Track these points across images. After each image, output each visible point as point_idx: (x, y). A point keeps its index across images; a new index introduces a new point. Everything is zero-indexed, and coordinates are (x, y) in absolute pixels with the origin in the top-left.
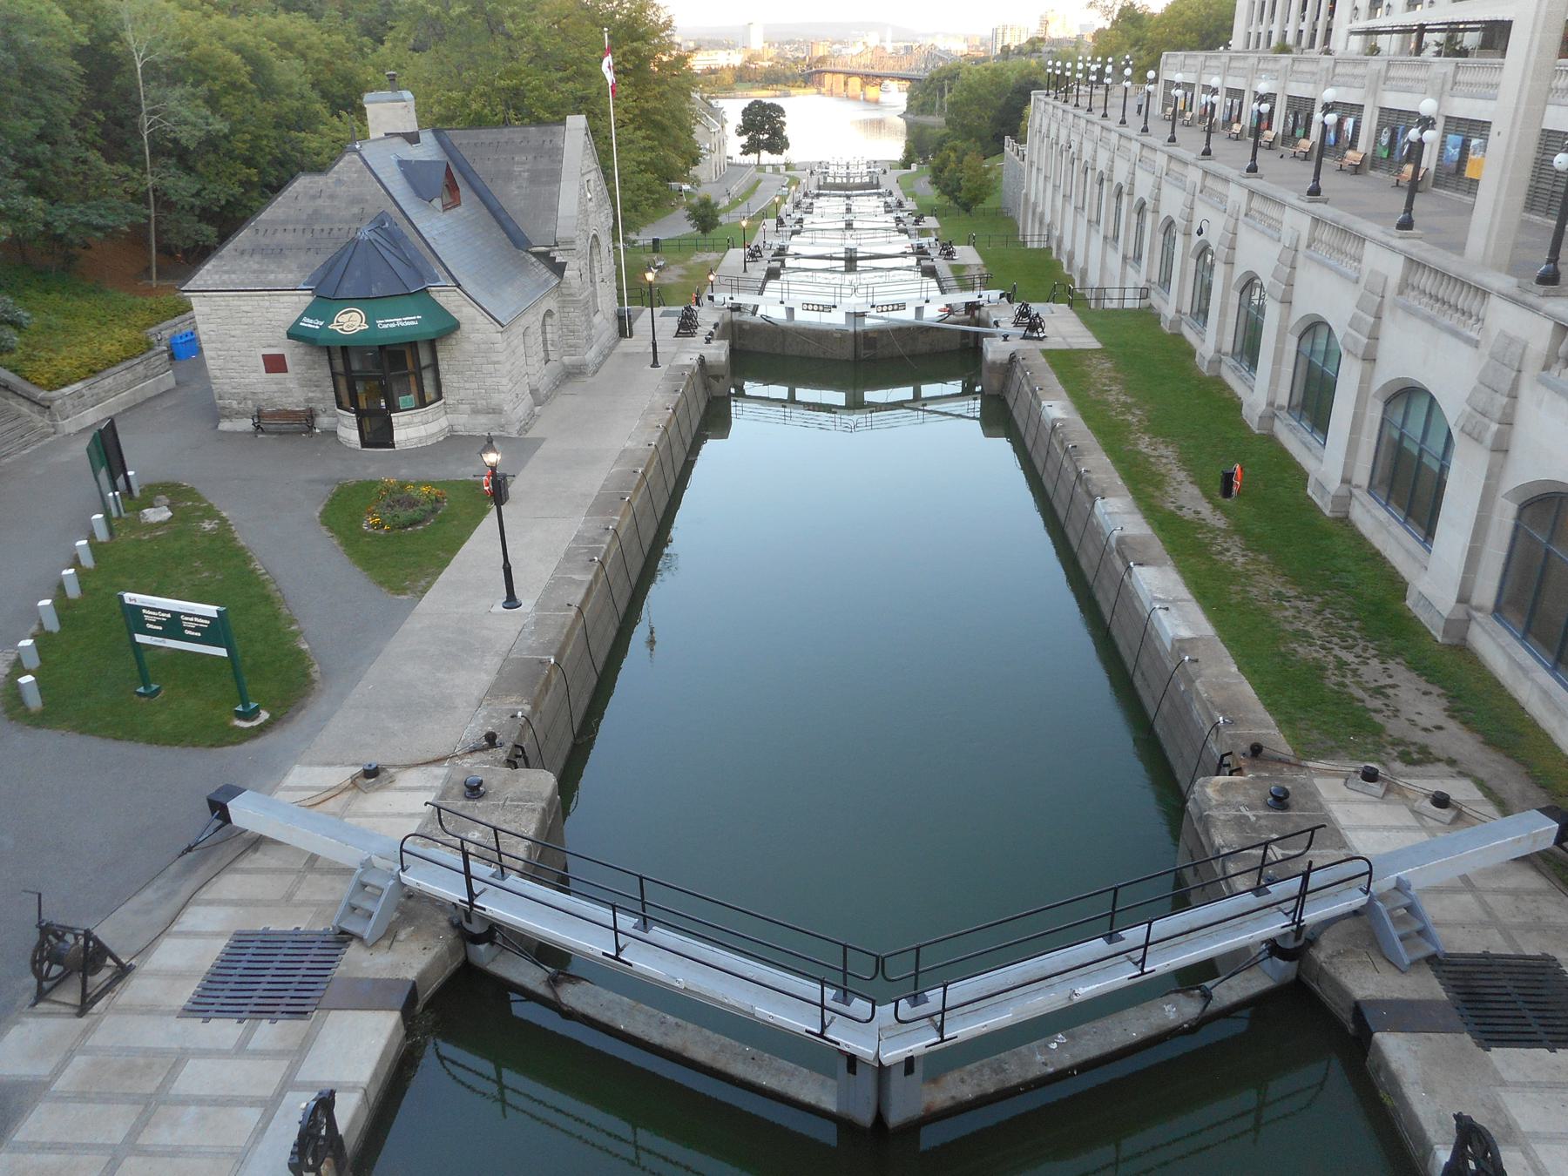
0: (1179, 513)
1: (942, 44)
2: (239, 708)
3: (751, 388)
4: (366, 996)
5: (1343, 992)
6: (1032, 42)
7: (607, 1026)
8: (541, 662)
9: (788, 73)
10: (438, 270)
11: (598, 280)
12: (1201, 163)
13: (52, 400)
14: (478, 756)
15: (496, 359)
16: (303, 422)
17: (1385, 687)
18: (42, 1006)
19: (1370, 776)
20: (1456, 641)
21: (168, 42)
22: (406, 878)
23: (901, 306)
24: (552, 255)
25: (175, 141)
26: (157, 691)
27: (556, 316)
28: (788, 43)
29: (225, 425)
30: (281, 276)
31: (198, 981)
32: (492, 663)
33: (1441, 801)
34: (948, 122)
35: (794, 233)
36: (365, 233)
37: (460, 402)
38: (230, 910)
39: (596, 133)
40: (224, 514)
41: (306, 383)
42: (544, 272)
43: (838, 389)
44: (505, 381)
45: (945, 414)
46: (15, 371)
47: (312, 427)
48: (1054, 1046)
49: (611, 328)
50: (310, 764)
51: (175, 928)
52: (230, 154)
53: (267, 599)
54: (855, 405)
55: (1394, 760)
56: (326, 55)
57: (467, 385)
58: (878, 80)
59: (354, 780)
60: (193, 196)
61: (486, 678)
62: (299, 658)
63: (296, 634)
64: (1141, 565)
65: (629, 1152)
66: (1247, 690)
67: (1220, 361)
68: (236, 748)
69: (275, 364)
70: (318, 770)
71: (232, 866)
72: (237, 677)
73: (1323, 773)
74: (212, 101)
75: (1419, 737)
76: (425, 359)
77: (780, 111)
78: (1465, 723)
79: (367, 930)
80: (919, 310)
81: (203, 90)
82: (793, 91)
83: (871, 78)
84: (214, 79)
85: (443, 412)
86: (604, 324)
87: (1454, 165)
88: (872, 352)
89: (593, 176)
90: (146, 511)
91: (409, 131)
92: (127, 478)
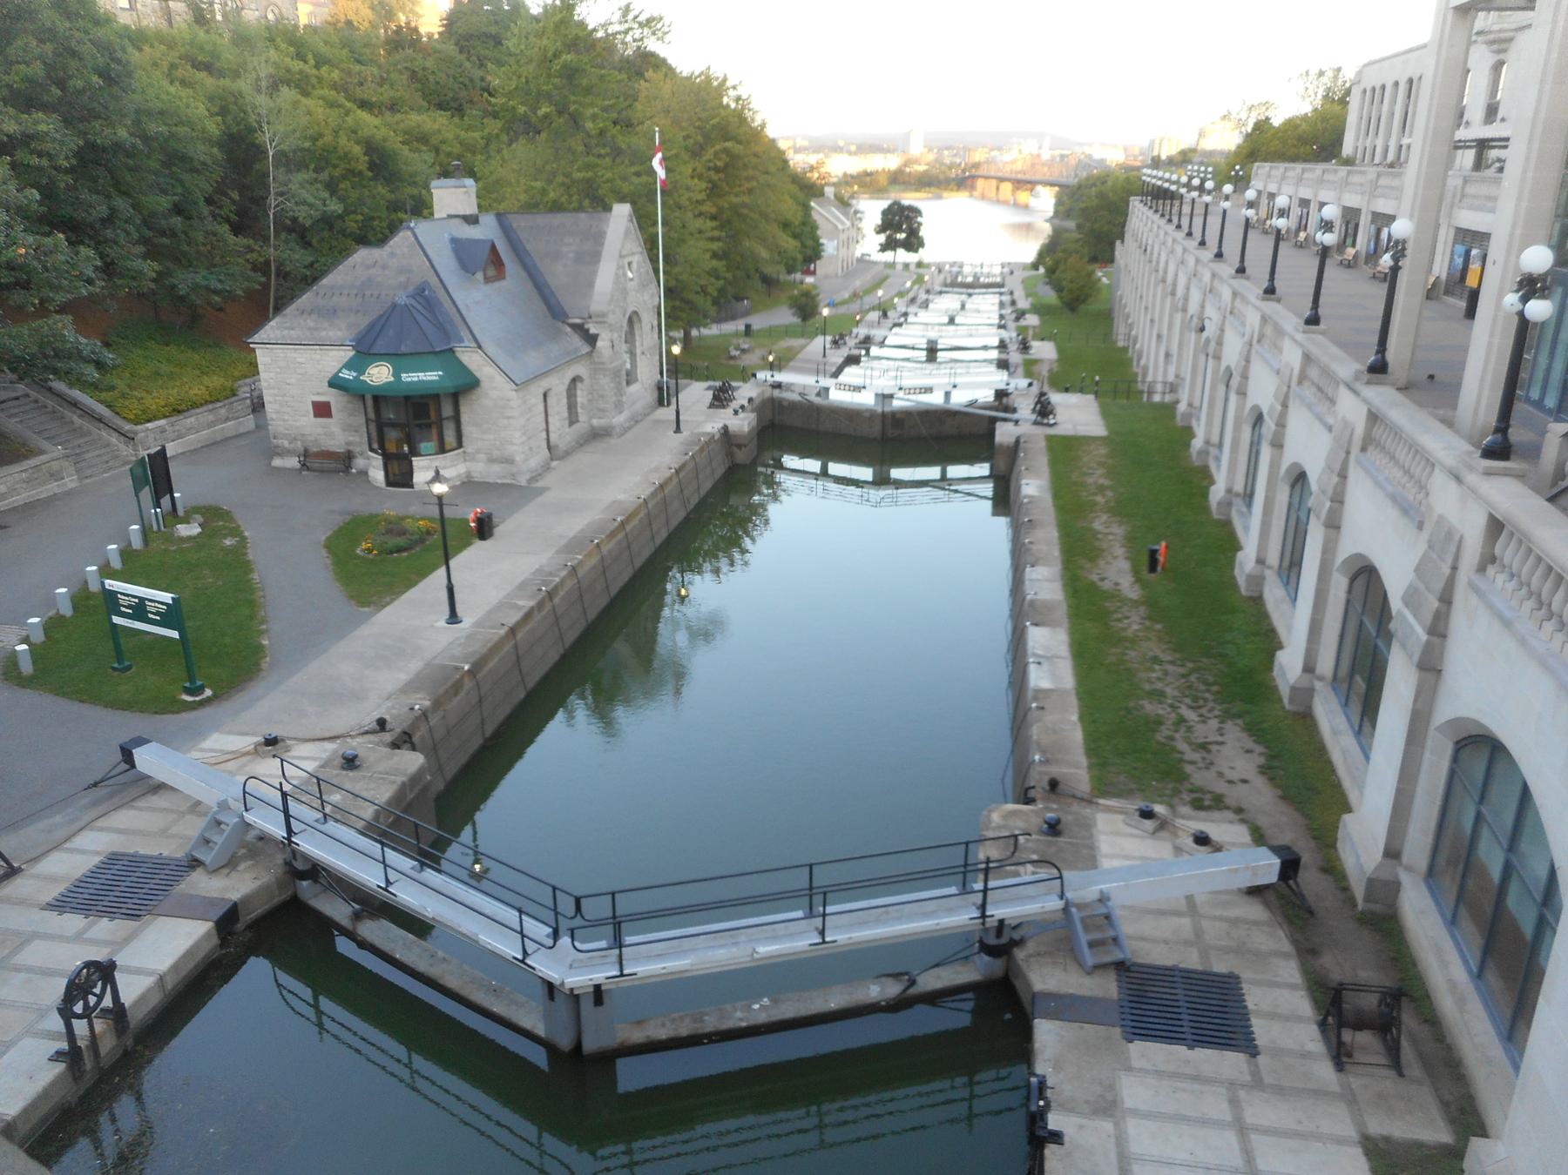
0: (1099, 583)
1: (1098, 154)
2: (187, 685)
3: (790, 461)
4: (189, 909)
5: (1028, 985)
6: (1184, 153)
7: (387, 954)
8: (457, 669)
9: (941, 177)
10: (464, 333)
11: (638, 351)
12: (1211, 264)
13: (136, 433)
16: (345, 460)
17: (1210, 743)
19: (1147, 814)
20: (1301, 709)
21: (298, 134)
22: (249, 817)
23: (929, 390)
25: (294, 220)
26: (129, 668)
27: (587, 381)
28: (947, 149)
30: (331, 334)
31: (67, 885)
32: (415, 666)
33: (1202, 840)
34: (1079, 227)
35: (895, 325)
36: (402, 299)
37: (478, 451)
38: (114, 836)
39: (643, 219)
40: (246, 534)
42: (576, 341)
44: (517, 434)
45: (969, 494)
46: (109, 407)
47: (349, 467)
48: (756, 1006)
49: (651, 396)
50: (229, 733)
51: (67, 845)
52: (343, 232)
53: (252, 603)
54: (882, 481)
55: (1185, 804)
56: (457, 149)
57: (485, 437)
58: (1029, 186)
59: (257, 745)
60: (306, 267)
61: (403, 677)
62: (258, 650)
63: (262, 632)
64: (1036, 625)
65: (405, 1073)
66: (1077, 736)
67: (1208, 453)
69: (322, 410)
70: (232, 738)
72: (187, 656)
73: (1109, 810)
74: (332, 187)
75: (1220, 787)
76: (447, 410)
77: (917, 212)
78: (1271, 779)
79: (206, 857)
80: (947, 394)
81: (324, 176)
82: (945, 194)
83: (1024, 183)
84: (335, 166)
86: (641, 392)
87: (1458, 274)
89: (636, 259)
90: (179, 526)
91: (468, 213)
92: (173, 498)
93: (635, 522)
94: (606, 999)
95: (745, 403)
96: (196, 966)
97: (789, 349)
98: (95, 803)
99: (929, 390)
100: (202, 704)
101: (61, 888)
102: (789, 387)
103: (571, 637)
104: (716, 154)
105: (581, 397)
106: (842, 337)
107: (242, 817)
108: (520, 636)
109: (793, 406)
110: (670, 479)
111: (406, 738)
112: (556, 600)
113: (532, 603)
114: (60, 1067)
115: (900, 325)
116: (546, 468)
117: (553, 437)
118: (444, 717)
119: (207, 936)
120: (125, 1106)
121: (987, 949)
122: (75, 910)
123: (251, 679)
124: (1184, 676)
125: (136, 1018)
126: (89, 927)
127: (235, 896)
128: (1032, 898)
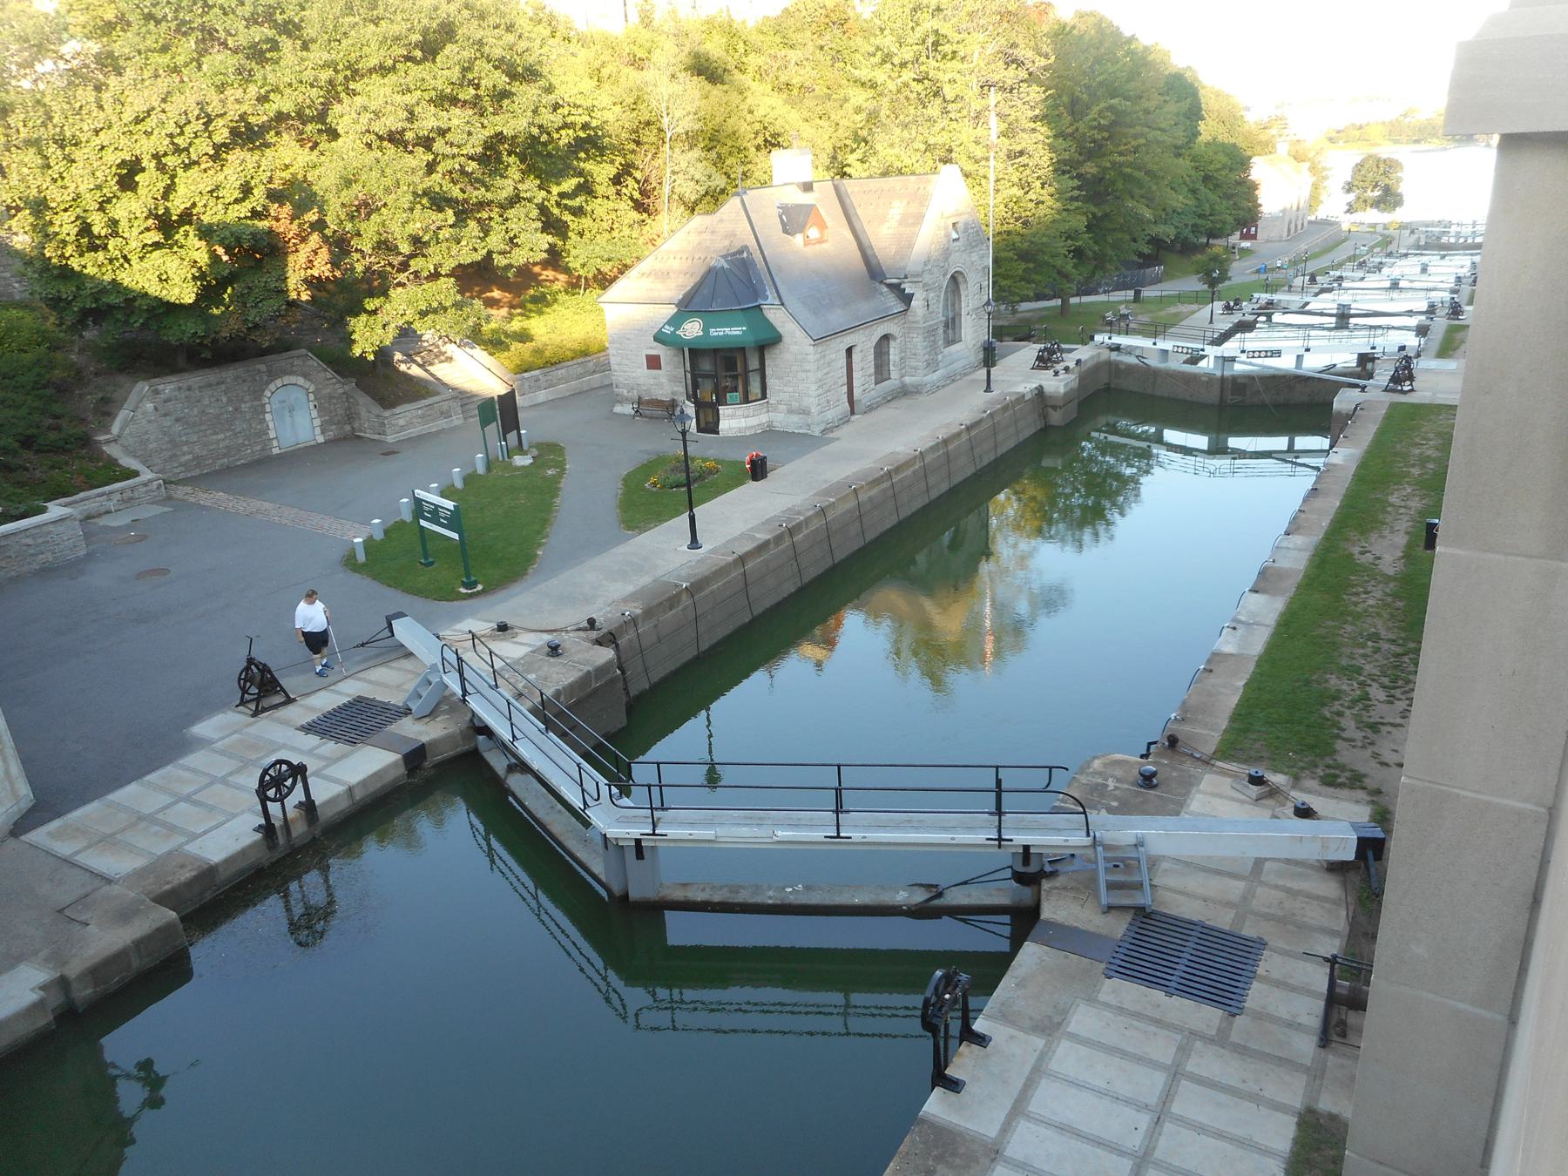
8: (676, 586)
14: (581, 634)
15: (808, 368)
16: (669, 409)
18: (241, 708)
19: (1257, 780)
23: (1277, 353)
24: (902, 286)
26: (432, 563)
29: (618, 409)
32: (645, 580)
37: (779, 402)
41: (672, 379)
43: (1202, 432)
50: (479, 620)
51: (332, 688)
53: (545, 522)
54: (1218, 450)
57: (785, 389)
61: (631, 588)
63: (540, 545)
68: (450, 603)
69: (653, 362)
71: (389, 664)
73: (1223, 772)
76: (754, 364)
80: (1300, 358)
81: (713, 154)
85: (765, 410)
88: (1240, 398)
92: (519, 435)
93: (909, 472)
94: (646, 854)
95: (1072, 365)
96: (383, 787)
97: (1176, 315)
98: (366, 660)
99: (1277, 353)
100: (471, 596)
101: (314, 717)
102: (1129, 351)
103: (811, 573)
104: (1100, 112)
105: (894, 353)
106: (1237, 302)
107: (441, 678)
108: (749, 566)
109: (1131, 369)
110: (959, 434)
111: (612, 637)
112: (798, 538)
113: (768, 537)
114: (259, 836)
115: (1329, 290)
116: (845, 420)
117: (857, 392)
118: (656, 626)
119: (395, 764)
120: (312, 878)
121: (1020, 878)
122: (316, 733)
123: (515, 581)
124: (1397, 655)
125: (325, 815)
126: (319, 746)
127: (425, 739)
128: (1058, 831)
